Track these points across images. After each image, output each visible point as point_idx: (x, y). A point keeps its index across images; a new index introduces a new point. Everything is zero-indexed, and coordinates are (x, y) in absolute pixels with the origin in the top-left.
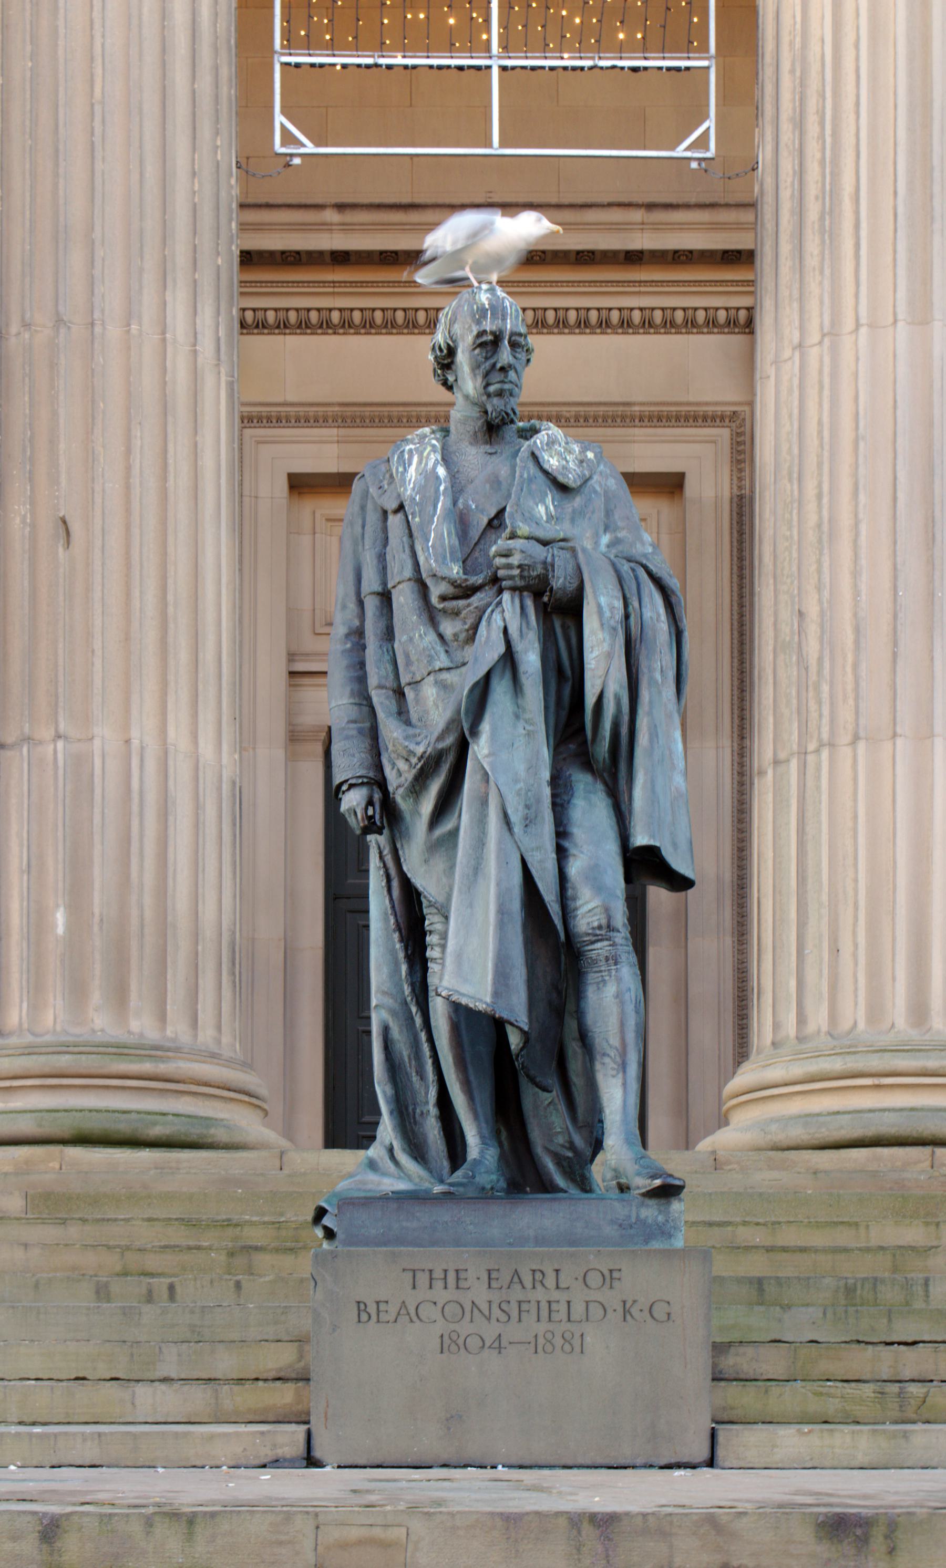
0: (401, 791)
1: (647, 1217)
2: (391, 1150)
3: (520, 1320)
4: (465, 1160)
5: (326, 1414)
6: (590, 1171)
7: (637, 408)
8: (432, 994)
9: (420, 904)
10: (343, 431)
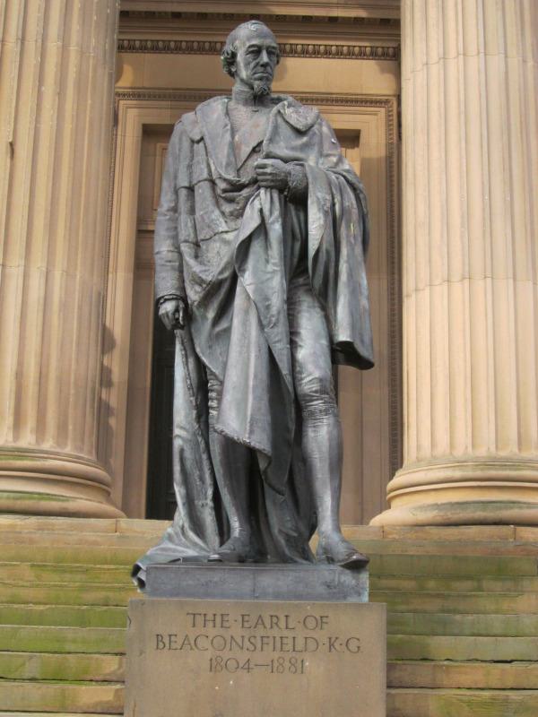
0: (196, 303)
1: (345, 581)
2: (183, 528)
3: (262, 650)
4: (229, 537)
5: (134, 711)
6: (308, 546)
7: (334, 96)
8: (211, 430)
9: (206, 373)
10: (173, 103)
